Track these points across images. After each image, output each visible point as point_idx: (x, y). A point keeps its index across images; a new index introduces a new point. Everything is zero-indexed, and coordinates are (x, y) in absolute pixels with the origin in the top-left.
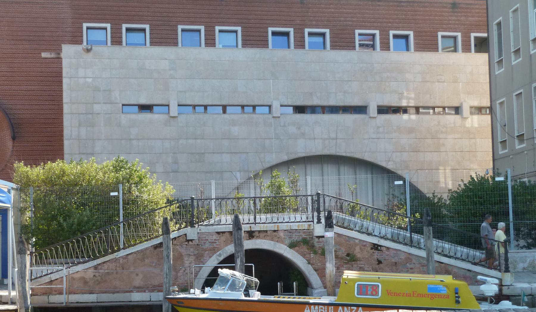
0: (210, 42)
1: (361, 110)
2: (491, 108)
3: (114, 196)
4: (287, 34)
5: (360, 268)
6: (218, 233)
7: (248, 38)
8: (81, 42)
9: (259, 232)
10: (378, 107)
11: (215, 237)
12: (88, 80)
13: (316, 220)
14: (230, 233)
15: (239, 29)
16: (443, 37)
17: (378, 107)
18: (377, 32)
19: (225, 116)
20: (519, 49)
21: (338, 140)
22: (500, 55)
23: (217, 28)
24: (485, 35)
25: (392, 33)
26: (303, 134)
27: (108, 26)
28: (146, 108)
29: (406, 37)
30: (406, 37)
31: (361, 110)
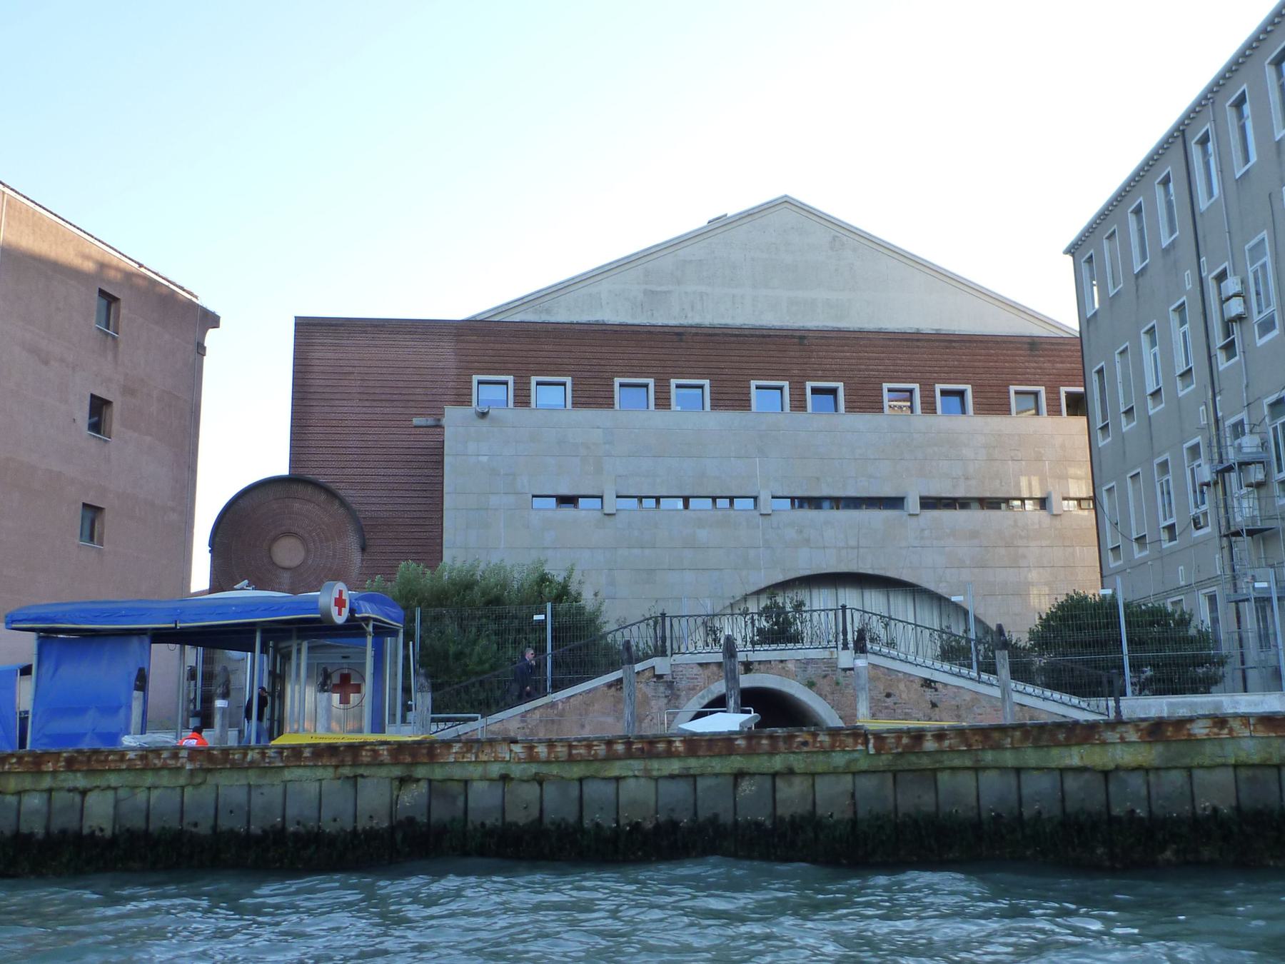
0: (663, 402)
1: (895, 503)
2: (1094, 499)
3: (539, 621)
4: (833, 392)
5: (906, 714)
6: (701, 665)
7: (720, 397)
8: (469, 403)
9: (760, 662)
10: (921, 498)
11: (697, 670)
12: (481, 458)
13: (840, 646)
14: (719, 664)
15: (706, 382)
16: (1017, 393)
17: (921, 498)
18: (916, 386)
19: (686, 512)
20: (1132, 408)
21: (861, 550)
22: (1104, 418)
23: (674, 382)
24: (1081, 389)
25: (938, 387)
26: (807, 541)
27: (510, 379)
28: (567, 500)
29: (961, 394)
30: (961, 394)
31: (895, 503)
